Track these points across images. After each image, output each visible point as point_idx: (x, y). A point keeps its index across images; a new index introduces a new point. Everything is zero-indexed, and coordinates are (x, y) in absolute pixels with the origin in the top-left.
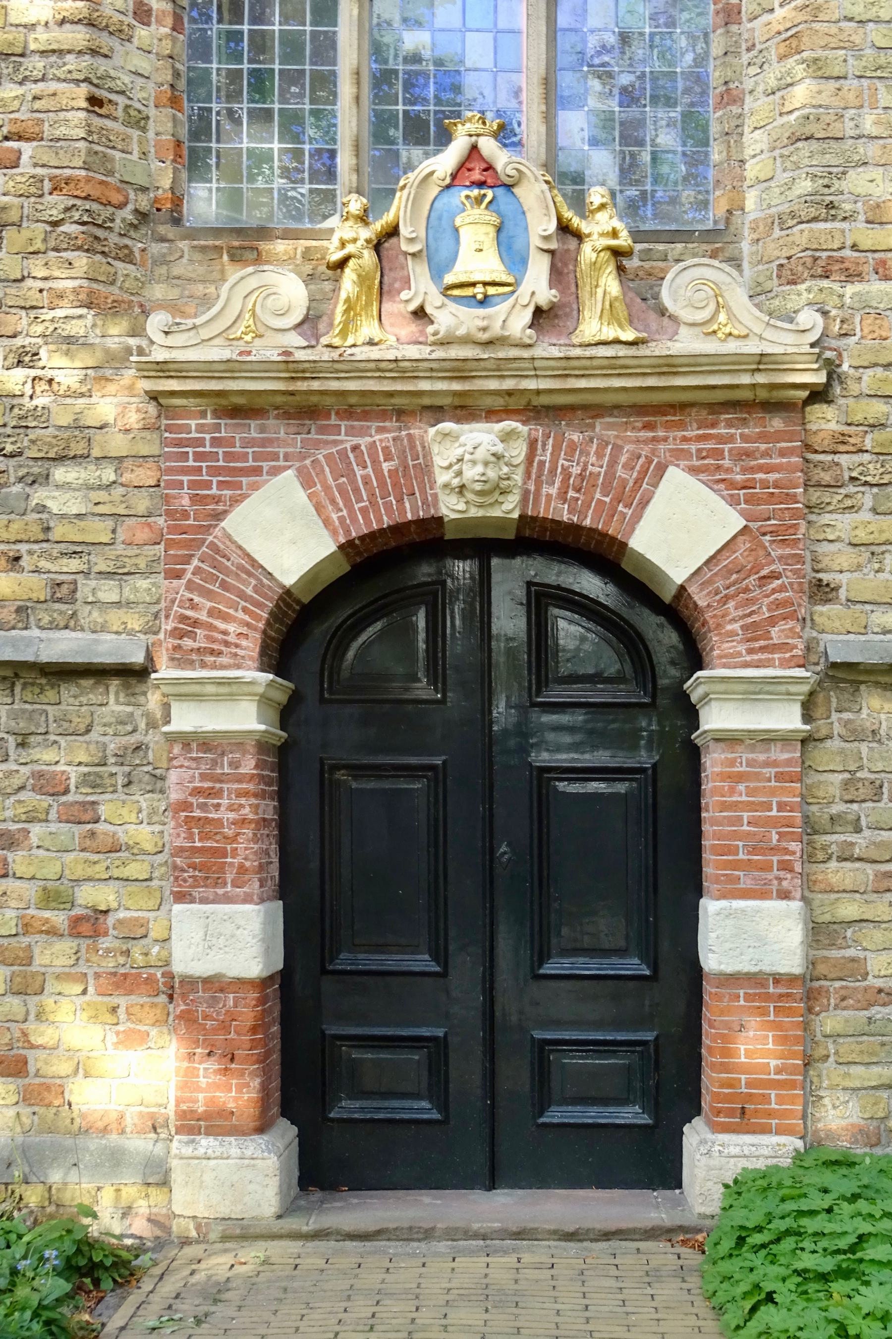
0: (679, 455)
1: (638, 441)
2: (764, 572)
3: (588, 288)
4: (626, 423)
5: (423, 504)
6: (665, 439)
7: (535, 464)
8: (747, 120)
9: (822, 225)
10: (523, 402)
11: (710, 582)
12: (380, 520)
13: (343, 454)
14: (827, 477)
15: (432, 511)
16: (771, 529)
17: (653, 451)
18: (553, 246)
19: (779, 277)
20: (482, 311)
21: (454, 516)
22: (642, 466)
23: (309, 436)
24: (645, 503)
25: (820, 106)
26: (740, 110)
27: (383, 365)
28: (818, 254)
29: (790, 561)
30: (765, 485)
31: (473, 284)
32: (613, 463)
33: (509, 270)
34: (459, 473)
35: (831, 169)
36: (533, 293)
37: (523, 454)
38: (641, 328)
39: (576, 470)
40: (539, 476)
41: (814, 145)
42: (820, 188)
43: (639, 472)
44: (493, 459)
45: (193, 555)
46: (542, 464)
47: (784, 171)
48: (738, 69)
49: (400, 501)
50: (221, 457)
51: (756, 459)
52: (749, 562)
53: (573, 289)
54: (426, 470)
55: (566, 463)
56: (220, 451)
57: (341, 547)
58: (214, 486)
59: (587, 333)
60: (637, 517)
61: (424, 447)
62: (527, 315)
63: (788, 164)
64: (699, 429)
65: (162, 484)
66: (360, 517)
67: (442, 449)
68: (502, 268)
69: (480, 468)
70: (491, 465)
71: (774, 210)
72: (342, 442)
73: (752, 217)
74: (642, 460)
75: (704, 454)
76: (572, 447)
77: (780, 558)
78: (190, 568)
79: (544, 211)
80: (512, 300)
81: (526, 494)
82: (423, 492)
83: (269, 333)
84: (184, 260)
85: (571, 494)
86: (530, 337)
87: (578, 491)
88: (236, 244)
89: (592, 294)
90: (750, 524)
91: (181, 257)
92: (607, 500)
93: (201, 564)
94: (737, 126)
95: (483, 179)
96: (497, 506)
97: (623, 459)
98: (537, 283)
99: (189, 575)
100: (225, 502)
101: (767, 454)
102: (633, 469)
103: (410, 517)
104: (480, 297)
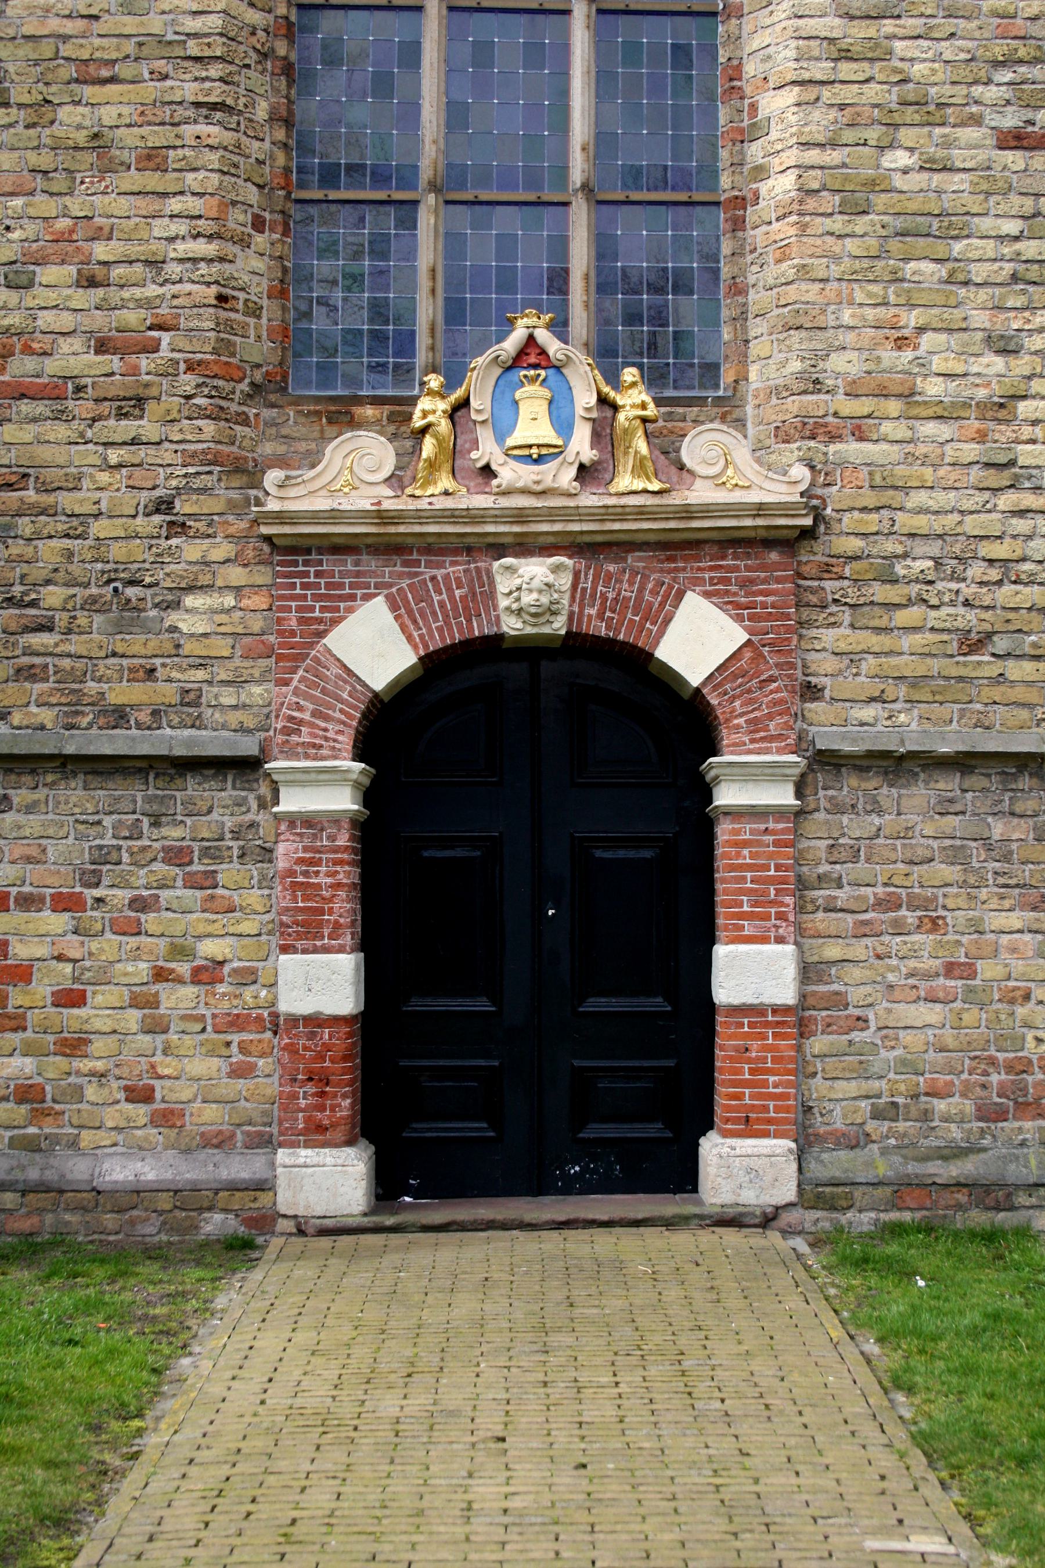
0: (696, 582)
1: (662, 571)
2: (763, 678)
3: (622, 448)
6: (684, 569)
11: (720, 685)
12: (453, 637)
14: (814, 599)
18: (594, 415)
19: (776, 436)
20: (536, 468)
24: (667, 621)
25: (808, 303)
27: (457, 513)
30: (764, 606)
31: (530, 446)
32: (641, 589)
33: (559, 433)
34: (518, 599)
39: (611, 596)
41: (803, 334)
46: (584, 590)
47: (780, 351)
49: (469, 621)
54: (491, 595)
56: (322, 581)
57: (421, 659)
60: (662, 633)
61: (489, 577)
62: (573, 472)
63: (783, 348)
68: (553, 433)
69: (535, 596)
71: (771, 383)
72: (422, 573)
73: (754, 386)
76: (609, 576)
77: (777, 665)
80: (561, 458)
83: (363, 486)
84: (291, 422)
85: (608, 614)
87: (614, 612)
88: (333, 408)
89: (626, 453)
90: (753, 638)
92: (637, 619)
97: (650, 586)
98: (581, 445)
99: (295, 683)
101: (765, 581)
103: (477, 634)
104: (535, 456)
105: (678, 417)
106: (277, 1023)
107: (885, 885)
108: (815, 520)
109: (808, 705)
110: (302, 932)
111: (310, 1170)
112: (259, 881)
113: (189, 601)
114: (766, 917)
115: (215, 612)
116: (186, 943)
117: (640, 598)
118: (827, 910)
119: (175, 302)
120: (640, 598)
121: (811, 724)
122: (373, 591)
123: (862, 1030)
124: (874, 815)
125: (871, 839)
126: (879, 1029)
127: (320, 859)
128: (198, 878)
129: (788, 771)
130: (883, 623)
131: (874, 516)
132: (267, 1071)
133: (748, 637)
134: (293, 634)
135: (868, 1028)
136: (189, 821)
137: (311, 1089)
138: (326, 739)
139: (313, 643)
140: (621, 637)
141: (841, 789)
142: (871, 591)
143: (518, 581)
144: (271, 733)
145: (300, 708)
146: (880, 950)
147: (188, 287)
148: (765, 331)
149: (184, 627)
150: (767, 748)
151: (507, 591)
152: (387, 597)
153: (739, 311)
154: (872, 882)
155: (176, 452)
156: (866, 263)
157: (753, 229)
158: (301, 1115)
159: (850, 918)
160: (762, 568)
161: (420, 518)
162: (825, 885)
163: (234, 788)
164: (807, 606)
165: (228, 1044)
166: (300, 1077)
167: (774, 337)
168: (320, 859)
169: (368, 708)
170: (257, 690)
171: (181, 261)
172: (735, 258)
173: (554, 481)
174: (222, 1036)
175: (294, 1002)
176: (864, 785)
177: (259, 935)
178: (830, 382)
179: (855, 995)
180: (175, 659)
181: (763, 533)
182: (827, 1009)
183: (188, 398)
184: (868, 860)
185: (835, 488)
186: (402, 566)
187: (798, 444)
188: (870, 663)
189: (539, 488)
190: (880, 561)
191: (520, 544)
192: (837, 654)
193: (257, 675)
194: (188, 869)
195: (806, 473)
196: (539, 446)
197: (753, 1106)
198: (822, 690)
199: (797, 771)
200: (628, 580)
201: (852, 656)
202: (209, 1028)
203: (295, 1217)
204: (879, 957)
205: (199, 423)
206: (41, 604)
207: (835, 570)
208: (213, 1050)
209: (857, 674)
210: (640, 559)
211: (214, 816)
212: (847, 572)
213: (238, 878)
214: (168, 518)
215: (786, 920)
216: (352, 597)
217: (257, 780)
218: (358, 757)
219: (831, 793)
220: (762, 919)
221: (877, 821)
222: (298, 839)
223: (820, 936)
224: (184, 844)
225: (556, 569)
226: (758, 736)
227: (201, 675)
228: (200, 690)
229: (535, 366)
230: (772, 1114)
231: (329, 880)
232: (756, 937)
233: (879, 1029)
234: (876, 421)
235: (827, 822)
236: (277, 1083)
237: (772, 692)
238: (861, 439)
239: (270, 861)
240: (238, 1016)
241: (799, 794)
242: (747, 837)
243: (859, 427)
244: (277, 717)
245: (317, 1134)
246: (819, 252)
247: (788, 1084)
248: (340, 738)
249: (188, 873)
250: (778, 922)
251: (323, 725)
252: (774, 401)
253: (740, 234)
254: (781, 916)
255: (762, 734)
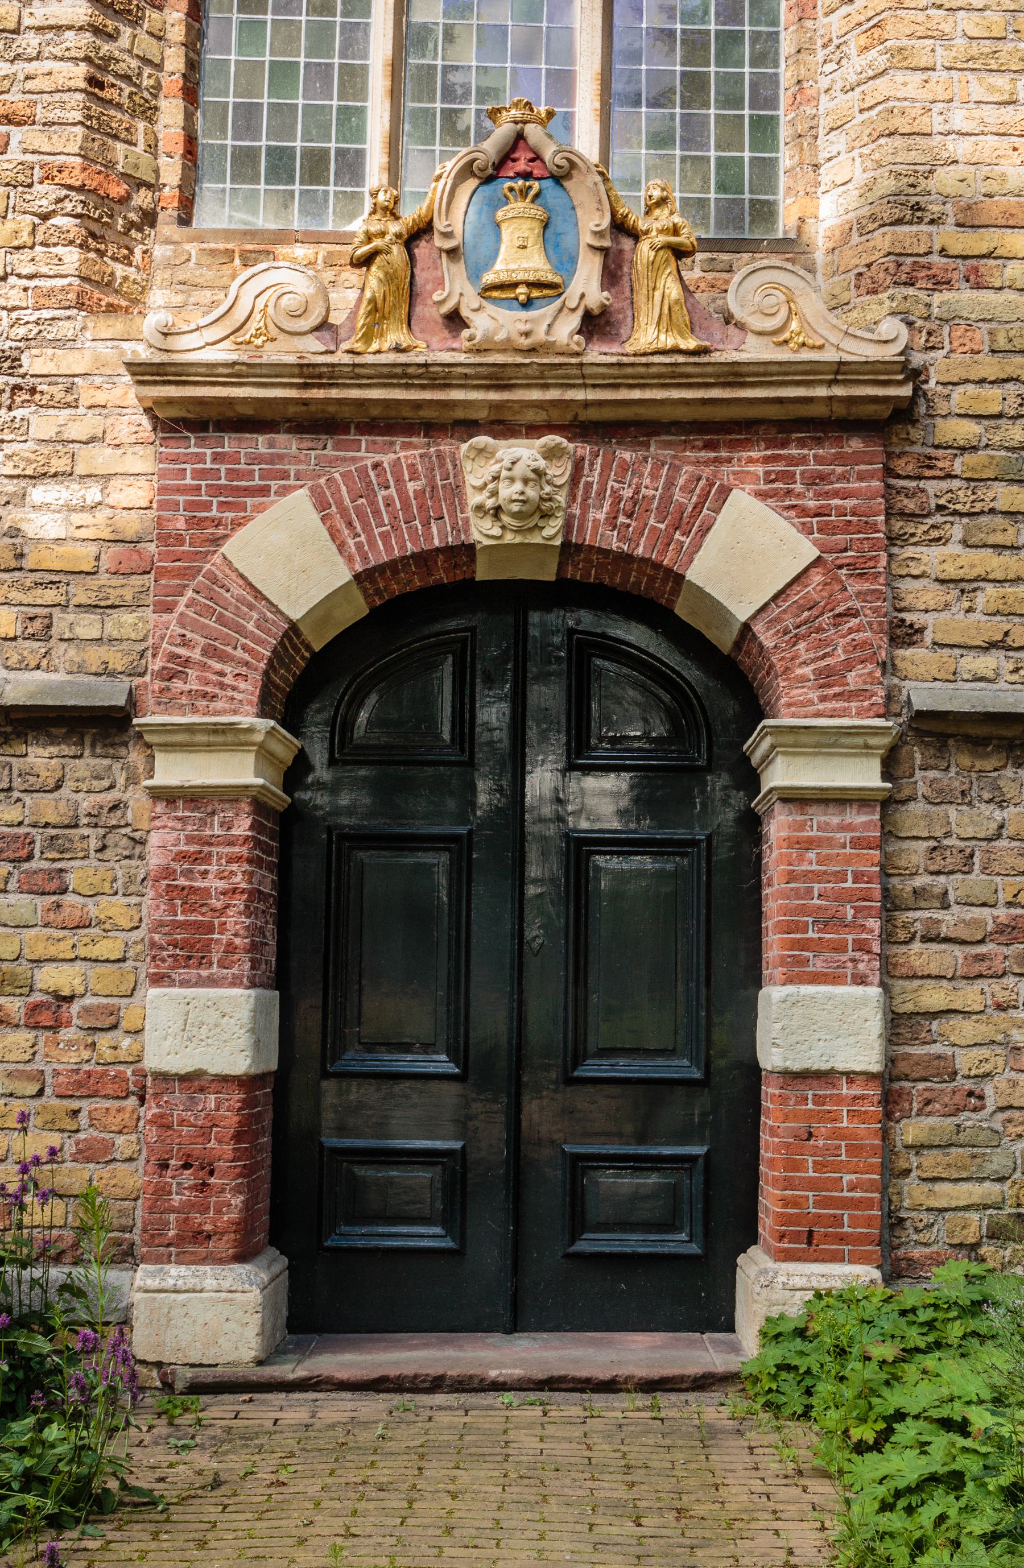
1: (698, 462)
2: (839, 610)
3: (644, 291)
4: (685, 441)
5: (453, 529)
6: (729, 461)
7: (581, 486)
8: (821, 121)
9: (906, 228)
10: (569, 417)
12: (403, 547)
13: (363, 472)
14: (910, 505)
15: (463, 537)
16: (848, 561)
17: (715, 474)
18: (607, 243)
20: (524, 314)
21: (487, 542)
22: (702, 489)
23: (325, 452)
25: (905, 99)
26: (814, 111)
27: (411, 370)
28: (901, 259)
29: (869, 598)
31: (515, 285)
32: (670, 484)
33: (556, 269)
34: (494, 494)
35: (917, 167)
36: (583, 296)
37: (568, 473)
38: (704, 336)
39: (627, 493)
40: (585, 499)
41: (898, 141)
42: (905, 187)
43: (699, 496)
44: (533, 476)
45: (187, 586)
46: (589, 485)
48: (813, 67)
49: (426, 525)
50: (223, 474)
51: (832, 483)
52: (823, 598)
53: (628, 293)
54: (456, 491)
55: (616, 485)
56: (223, 468)
57: (357, 577)
58: (214, 507)
59: (642, 340)
60: (697, 547)
62: (574, 321)
64: (766, 449)
65: (155, 505)
66: (380, 543)
67: (476, 466)
68: (548, 267)
69: (518, 486)
70: (531, 483)
72: (362, 459)
74: (702, 483)
75: (773, 477)
76: (624, 467)
77: (858, 594)
78: (184, 600)
79: (596, 205)
81: (568, 527)
82: (453, 516)
83: (282, 336)
84: (191, 264)
85: (622, 519)
86: (578, 344)
87: (630, 516)
88: (250, 247)
89: (650, 298)
91: (189, 260)
92: (662, 526)
93: (195, 596)
94: (812, 128)
95: (529, 169)
96: (537, 532)
97: (681, 481)
98: (586, 284)
99: (181, 608)
100: (226, 525)
101: (844, 477)
102: (693, 491)
103: (437, 543)
104: (522, 298)
105: (721, 266)
106: (146, 1086)
107: (1009, 904)
108: (915, 390)
109: (901, 652)
110: (183, 953)
111: (182, 1297)
112: (126, 886)
113: (39, 494)
114: (840, 948)
115: (71, 509)
116: (19, 969)
117: (667, 499)
118: (926, 939)
119: (30, 85)
120: (667, 499)
121: (905, 678)
122: (292, 482)
123: (975, 1110)
124: (992, 807)
125: (989, 840)
126: (1002, 1109)
127: (210, 854)
128: (39, 879)
129: (873, 741)
130: (1007, 539)
131: (997, 392)
132: (128, 1153)
133: (818, 553)
134: (180, 540)
135: (983, 1107)
136: (27, 799)
137: (188, 1178)
138: (222, 686)
139: (207, 553)
140: (640, 551)
141: (947, 769)
142: (991, 494)
143: (496, 467)
144: (148, 678)
145: (185, 643)
146: (1002, 996)
147: (48, 65)
148: (842, 147)
149: (30, 530)
150: (845, 709)
151: (479, 483)
152: (312, 490)
153: (806, 126)
154: (991, 902)
155: (25, 290)
156: (987, 46)
157: (827, 15)
158: (172, 1217)
159: (958, 951)
160: (840, 459)
161: (358, 376)
162: (923, 904)
163: (94, 755)
164: (901, 519)
165: (76, 1113)
166: (173, 1162)
167: (856, 153)
168: (210, 854)
169: (281, 643)
170: (128, 618)
171: (40, 29)
172: (800, 56)
173: (548, 333)
174: (65, 1103)
175: (165, 1051)
176: (979, 765)
177: (123, 960)
178: (935, 208)
179: (965, 1061)
180: (17, 574)
181: (840, 411)
182: (925, 1080)
183: (45, 217)
184: (984, 869)
185: (944, 352)
186: (334, 449)
187: (890, 291)
188: (987, 596)
189: (525, 343)
190: (1003, 453)
191: (500, 422)
192: (942, 582)
193: (129, 597)
194: (25, 866)
195: (904, 330)
196: (530, 285)
197: (820, 1216)
198: (921, 630)
199: (886, 741)
200: (647, 473)
201: (963, 585)
202: (48, 1091)
203: (159, 1365)
204: (1000, 1007)
205: (59, 250)
206: (507, 482)
207: (940, 464)
208: (53, 1121)
209: (969, 610)
210: (668, 445)
211: (65, 792)
212: (958, 468)
213: (95, 880)
214: (13, 381)
215: (869, 952)
216: (264, 491)
217: (125, 744)
218: (262, 714)
219: (931, 774)
220: (835, 950)
221: (998, 815)
222: (179, 826)
223: (915, 977)
224: (22, 830)
225: (551, 454)
226: (831, 691)
227: (50, 596)
228: (50, 616)
229: (527, 176)
230: (846, 1229)
231: (221, 884)
232: (826, 975)
233: (1002, 1109)
234: (1000, 262)
235: (927, 816)
236: (141, 1171)
237: (851, 631)
238: (978, 286)
239: (141, 858)
240: (89, 1074)
241: (886, 776)
242: (814, 833)
243: (976, 269)
244: (154, 656)
245: (191, 1243)
246: (921, 31)
247: (870, 1186)
248: (242, 685)
249: (25, 872)
250: (858, 955)
251: (218, 666)
252: (855, 239)
253: (809, 24)
254: (862, 946)
255: (837, 689)
